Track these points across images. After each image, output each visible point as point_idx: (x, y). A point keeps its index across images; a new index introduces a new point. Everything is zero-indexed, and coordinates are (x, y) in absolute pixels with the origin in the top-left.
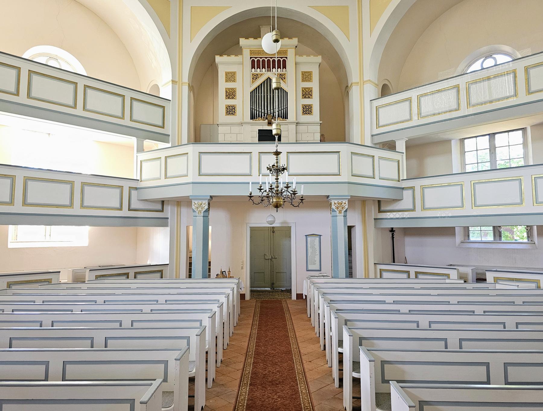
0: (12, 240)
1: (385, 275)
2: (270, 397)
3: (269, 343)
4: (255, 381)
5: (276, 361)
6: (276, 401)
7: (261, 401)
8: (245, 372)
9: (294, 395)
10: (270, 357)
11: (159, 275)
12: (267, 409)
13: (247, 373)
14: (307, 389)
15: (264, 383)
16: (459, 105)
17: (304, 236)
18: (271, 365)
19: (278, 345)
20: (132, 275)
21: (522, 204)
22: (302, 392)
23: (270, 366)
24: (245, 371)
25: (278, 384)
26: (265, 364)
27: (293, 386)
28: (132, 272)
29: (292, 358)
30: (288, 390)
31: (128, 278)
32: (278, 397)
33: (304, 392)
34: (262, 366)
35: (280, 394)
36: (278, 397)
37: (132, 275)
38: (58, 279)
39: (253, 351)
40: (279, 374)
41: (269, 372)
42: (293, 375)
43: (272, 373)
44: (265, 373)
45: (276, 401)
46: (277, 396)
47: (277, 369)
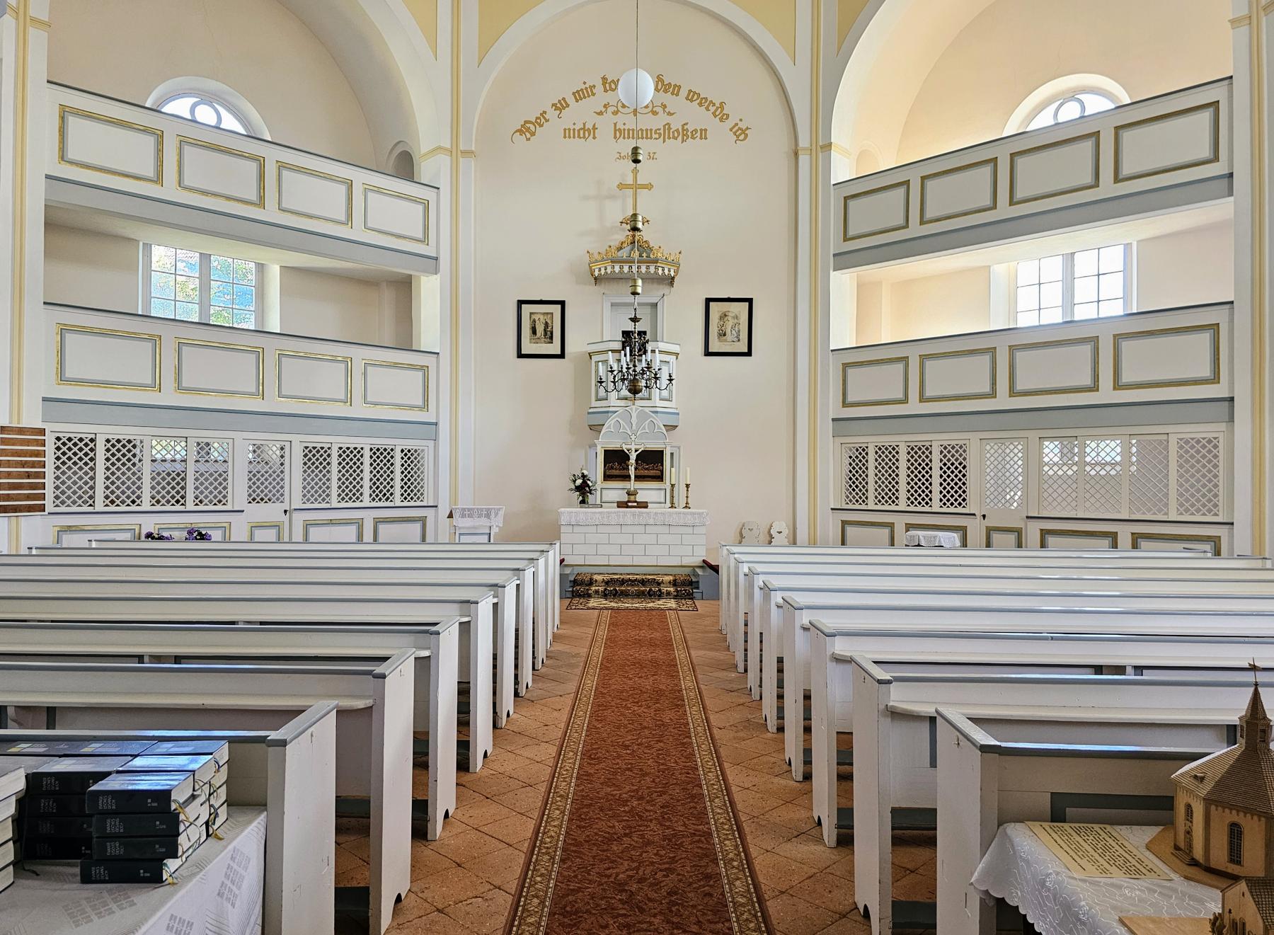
0: (53, 543)
1: (315, 534)
2: (651, 885)
3: (653, 781)
4: (687, 777)
5: (630, 773)
6: (632, 794)
7: (679, 875)
8: (717, 771)
9: (586, 805)
10: (652, 863)
11: (1012, 537)
12: (658, 850)
13: (716, 800)
14: (554, 786)
15: (663, 772)
16: (146, 130)
17: (267, 210)
18: (647, 826)
19: (625, 727)
20: (1125, 539)
21: (61, 380)
22: (542, 903)
23: (648, 760)
24: (718, 776)
25: (628, 769)
26: (663, 764)
27: (590, 764)
28: (1125, 533)
29: (588, 733)
30: (605, 758)
31: (1115, 545)
32: (627, 801)
33: (536, 901)
34: (677, 822)
35: (623, 809)
36: (627, 801)
37: (1125, 539)
38: (635, 498)
39: (713, 810)
40: (624, 742)
41: (649, 747)
42: (569, 867)
43: (646, 879)
44: (664, 796)
45: (632, 794)
46: (629, 804)
47: (628, 751)
